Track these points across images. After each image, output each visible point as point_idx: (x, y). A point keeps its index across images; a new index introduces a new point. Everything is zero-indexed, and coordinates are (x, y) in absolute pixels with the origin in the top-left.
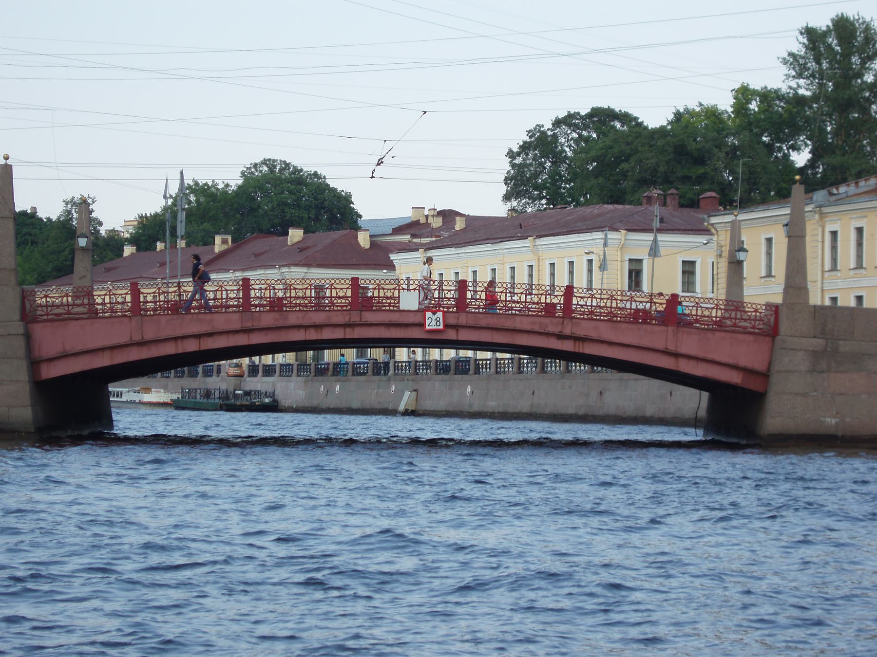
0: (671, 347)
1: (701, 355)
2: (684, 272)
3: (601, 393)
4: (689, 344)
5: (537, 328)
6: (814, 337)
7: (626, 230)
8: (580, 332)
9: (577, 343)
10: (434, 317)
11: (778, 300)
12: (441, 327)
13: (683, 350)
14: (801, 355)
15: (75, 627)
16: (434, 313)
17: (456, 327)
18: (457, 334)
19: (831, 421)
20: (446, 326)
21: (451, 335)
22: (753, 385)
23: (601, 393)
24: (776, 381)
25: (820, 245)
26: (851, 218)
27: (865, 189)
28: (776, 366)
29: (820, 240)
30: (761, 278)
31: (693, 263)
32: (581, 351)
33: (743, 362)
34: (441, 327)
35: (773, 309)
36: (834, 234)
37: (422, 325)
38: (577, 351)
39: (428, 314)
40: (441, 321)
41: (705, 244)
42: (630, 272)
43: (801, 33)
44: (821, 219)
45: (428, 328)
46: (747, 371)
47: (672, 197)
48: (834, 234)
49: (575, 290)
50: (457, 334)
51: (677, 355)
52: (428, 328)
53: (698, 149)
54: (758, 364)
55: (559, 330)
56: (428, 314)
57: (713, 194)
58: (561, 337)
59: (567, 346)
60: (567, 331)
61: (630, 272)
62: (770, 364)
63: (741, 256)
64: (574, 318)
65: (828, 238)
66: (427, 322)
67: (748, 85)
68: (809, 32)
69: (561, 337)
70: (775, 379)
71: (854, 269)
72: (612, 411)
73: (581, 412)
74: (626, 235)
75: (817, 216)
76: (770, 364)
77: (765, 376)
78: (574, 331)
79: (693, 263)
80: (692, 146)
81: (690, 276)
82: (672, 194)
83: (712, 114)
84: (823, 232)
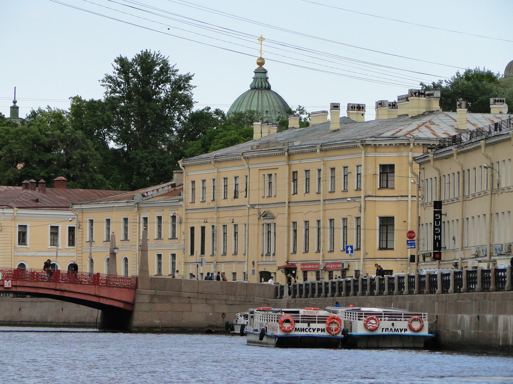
0: (97, 294)
1: (108, 296)
2: (51, 233)
3: (20, 309)
4: (104, 292)
5: (46, 287)
6: (151, 289)
7: (17, 207)
8: (63, 288)
9: (61, 292)
10: (8, 282)
11: (137, 274)
12: (10, 286)
13: (101, 295)
14: (146, 296)
15: (432, 263)
16: (8, 281)
17: (16, 286)
18: (16, 289)
19: (157, 322)
20: (12, 286)
21: (14, 289)
22: (128, 308)
23: (20, 309)
24: (137, 307)
25: (138, 224)
26: (155, 211)
27: (162, 193)
28: (137, 301)
29: (138, 222)
30: (104, 242)
31: (57, 227)
32: (63, 295)
33: (124, 299)
34: (10, 286)
35: (135, 278)
36: (146, 219)
37: (3, 286)
38: (61, 295)
39: (6, 281)
40: (10, 284)
41: (71, 221)
42: (19, 233)
43: (116, 61)
44: (138, 210)
45: (5, 286)
46: (125, 302)
47: (42, 184)
48: (146, 219)
49: (61, 272)
50: (16, 289)
51: (99, 297)
52: (5, 286)
53: (49, 142)
54: (129, 300)
55: (55, 287)
56: (6, 281)
57: (63, 178)
58: (56, 290)
59: (58, 293)
60: (58, 288)
61: (19, 233)
62: (134, 300)
63: (116, 251)
64: (60, 282)
65: (142, 220)
66: (5, 285)
67: (81, 97)
68: (121, 61)
69: (56, 290)
70: (136, 306)
71: (156, 239)
72: (27, 319)
73: (8, 319)
74: (17, 211)
75: (136, 209)
76: (134, 300)
77: (132, 304)
78: (60, 288)
79: (57, 227)
80: (45, 140)
81: (55, 236)
82: (42, 183)
83: (58, 116)
84: (139, 218)
